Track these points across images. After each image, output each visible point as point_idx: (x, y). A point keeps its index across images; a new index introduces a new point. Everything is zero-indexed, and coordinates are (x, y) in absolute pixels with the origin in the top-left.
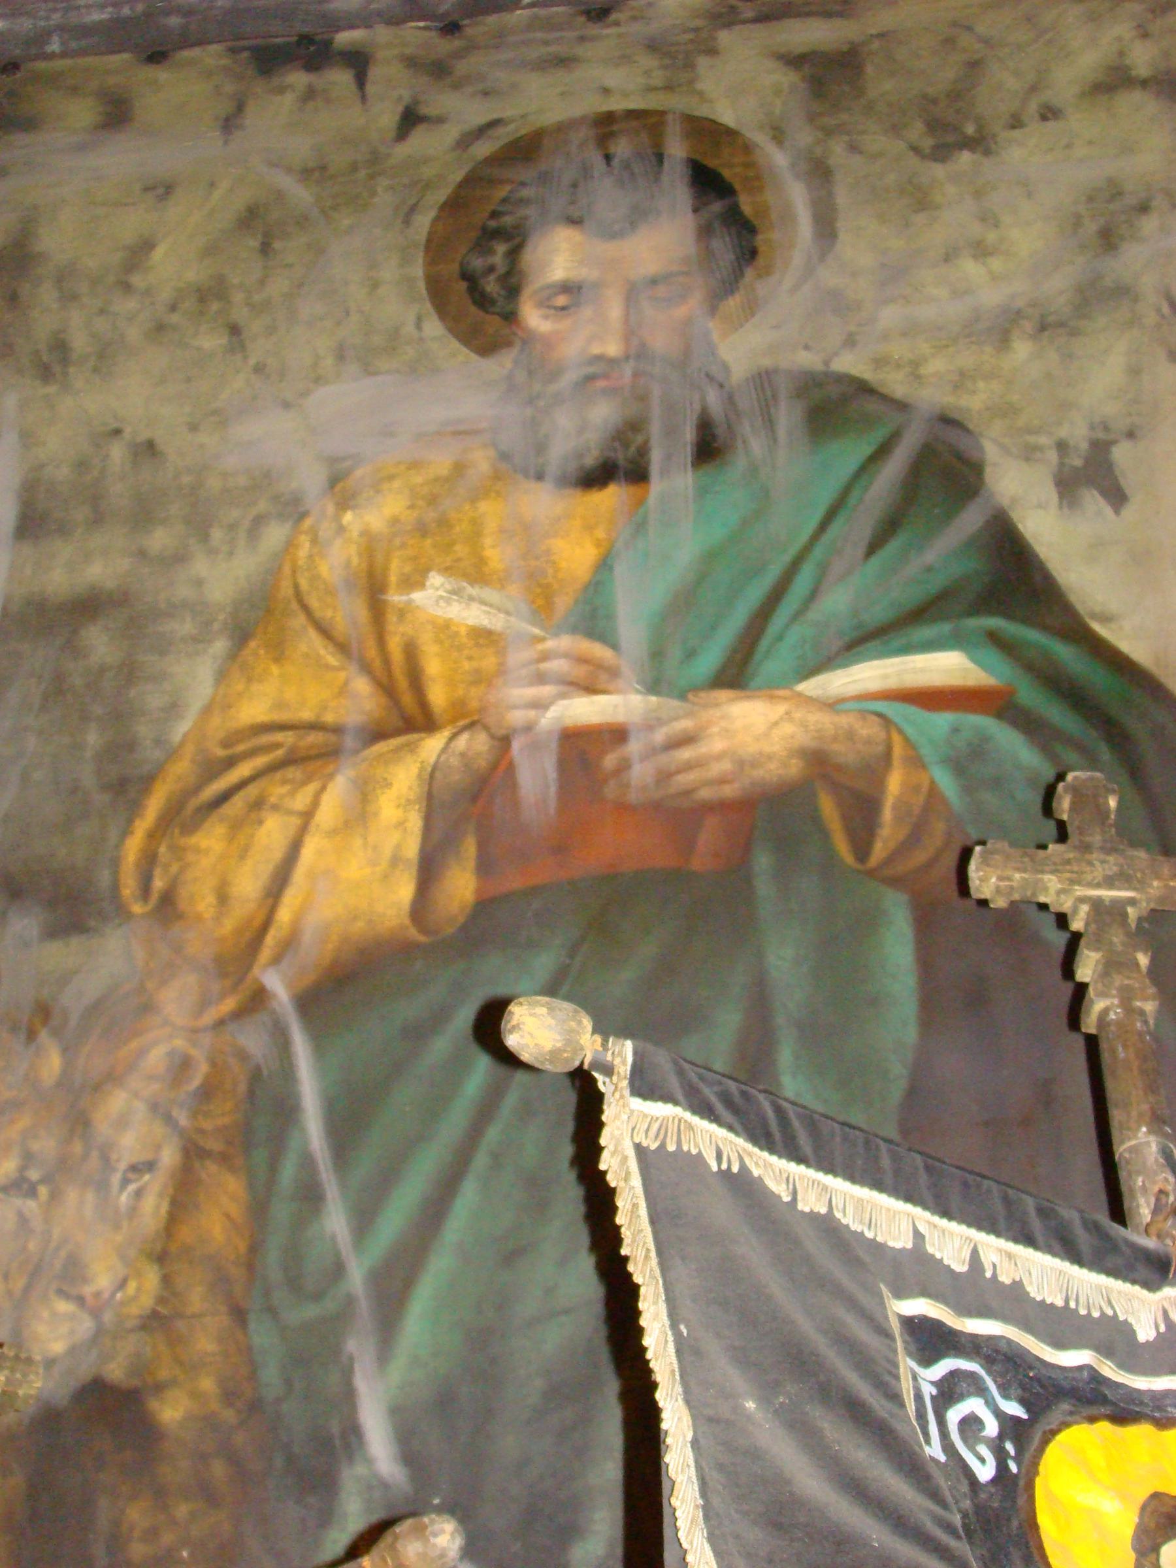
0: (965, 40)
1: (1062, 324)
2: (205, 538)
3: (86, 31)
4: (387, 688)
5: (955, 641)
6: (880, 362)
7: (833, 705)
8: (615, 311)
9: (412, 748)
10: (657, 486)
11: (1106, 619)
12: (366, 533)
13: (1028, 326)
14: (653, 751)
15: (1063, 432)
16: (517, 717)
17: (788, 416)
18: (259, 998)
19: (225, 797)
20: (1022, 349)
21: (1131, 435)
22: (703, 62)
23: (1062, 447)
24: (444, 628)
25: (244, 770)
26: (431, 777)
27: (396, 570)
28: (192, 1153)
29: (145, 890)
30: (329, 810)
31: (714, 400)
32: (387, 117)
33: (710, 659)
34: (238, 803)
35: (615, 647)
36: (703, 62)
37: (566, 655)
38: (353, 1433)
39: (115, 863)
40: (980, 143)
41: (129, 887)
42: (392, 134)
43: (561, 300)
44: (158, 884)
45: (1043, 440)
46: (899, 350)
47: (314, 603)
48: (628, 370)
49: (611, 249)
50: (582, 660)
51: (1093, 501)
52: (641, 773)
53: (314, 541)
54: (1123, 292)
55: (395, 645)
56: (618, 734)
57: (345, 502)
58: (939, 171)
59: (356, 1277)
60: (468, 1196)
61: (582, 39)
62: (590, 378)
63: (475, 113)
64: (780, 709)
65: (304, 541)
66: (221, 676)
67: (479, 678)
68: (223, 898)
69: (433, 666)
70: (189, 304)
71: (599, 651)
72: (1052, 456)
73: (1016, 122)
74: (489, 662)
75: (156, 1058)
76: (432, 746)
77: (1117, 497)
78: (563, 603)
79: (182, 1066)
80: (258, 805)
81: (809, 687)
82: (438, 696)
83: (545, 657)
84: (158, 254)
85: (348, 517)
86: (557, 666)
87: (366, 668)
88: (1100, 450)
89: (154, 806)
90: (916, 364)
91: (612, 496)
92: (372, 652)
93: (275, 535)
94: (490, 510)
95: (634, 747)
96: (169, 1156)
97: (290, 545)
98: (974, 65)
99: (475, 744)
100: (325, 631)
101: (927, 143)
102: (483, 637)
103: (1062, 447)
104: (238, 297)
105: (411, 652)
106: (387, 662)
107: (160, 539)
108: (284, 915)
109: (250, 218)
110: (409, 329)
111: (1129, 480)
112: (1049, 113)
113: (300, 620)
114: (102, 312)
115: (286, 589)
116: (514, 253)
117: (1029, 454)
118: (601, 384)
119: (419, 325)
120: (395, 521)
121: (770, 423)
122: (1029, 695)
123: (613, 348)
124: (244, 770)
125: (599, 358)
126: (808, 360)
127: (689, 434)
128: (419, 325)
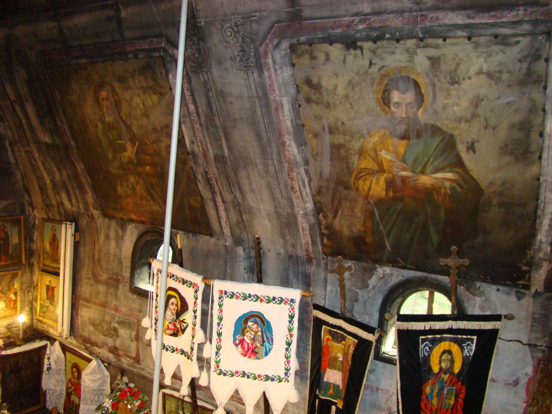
0: (457, 59)
1: (469, 121)
2: (353, 139)
3: (320, 39)
4: (379, 165)
5: (452, 172)
6: (442, 124)
7: (435, 179)
8: (404, 109)
9: (383, 175)
10: (411, 142)
11: (471, 171)
12: (373, 142)
13: (464, 120)
14: (412, 181)
15: (468, 140)
16: (395, 173)
17: (429, 132)
18: (369, 203)
19: (362, 177)
20: (463, 124)
21: (477, 141)
22: (415, 56)
23: (467, 142)
24: (385, 158)
25: (363, 174)
26: (386, 179)
27: (378, 149)
28: (365, 217)
29: (354, 187)
30: (374, 180)
31: (419, 127)
32: (367, 63)
33: (419, 169)
34: (363, 178)
35: (407, 165)
36: (415, 56)
37: (401, 165)
38: (386, 247)
39: (350, 182)
40: (458, 83)
41: (353, 186)
42: (368, 67)
43: (396, 105)
44: (356, 186)
45: (465, 141)
46: (445, 122)
47: (368, 151)
48: (406, 120)
49: (403, 96)
50: (403, 166)
51: (471, 152)
52: (412, 184)
53: (367, 142)
54: (478, 116)
55: (379, 160)
56: (408, 178)
57: (370, 137)
58: (452, 87)
59: (384, 233)
60: (395, 227)
61: (396, 48)
62: (401, 121)
63: (381, 64)
64: (428, 178)
65: (366, 142)
66: (358, 160)
67: (390, 167)
68: (364, 190)
69: (384, 164)
70: (344, 98)
71: (405, 166)
72: (466, 143)
73: (464, 79)
74: (391, 164)
75: (359, 206)
76: (386, 175)
77: (474, 152)
78: (400, 157)
79: (362, 208)
80: (366, 179)
81: (432, 175)
82: (386, 168)
83: (399, 165)
84: (338, 88)
85: (371, 139)
86: (400, 166)
87: (376, 163)
88: (473, 143)
89: (354, 176)
90: (447, 125)
91: (405, 142)
92: (377, 161)
93: (362, 140)
94: (389, 141)
95: (411, 180)
96: (363, 217)
97: (364, 142)
98: (458, 64)
99: (390, 175)
100: (370, 156)
101: (450, 81)
102: (390, 161)
103: (467, 142)
104: (351, 98)
105: (381, 160)
106: (378, 161)
107: (347, 138)
108: (371, 193)
109: (350, 82)
110: (375, 107)
111: (476, 150)
112: (469, 78)
113: (367, 154)
114: (333, 98)
115: (364, 149)
116: (389, 95)
117: (463, 143)
118: (403, 122)
119: (376, 107)
120: (377, 141)
121: (427, 133)
122: (461, 182)
123: (404, 116)
124: (363, 174)
125: (402, 117)
126: (432, 122)
127: (415, 133)
128: (376, 107)
